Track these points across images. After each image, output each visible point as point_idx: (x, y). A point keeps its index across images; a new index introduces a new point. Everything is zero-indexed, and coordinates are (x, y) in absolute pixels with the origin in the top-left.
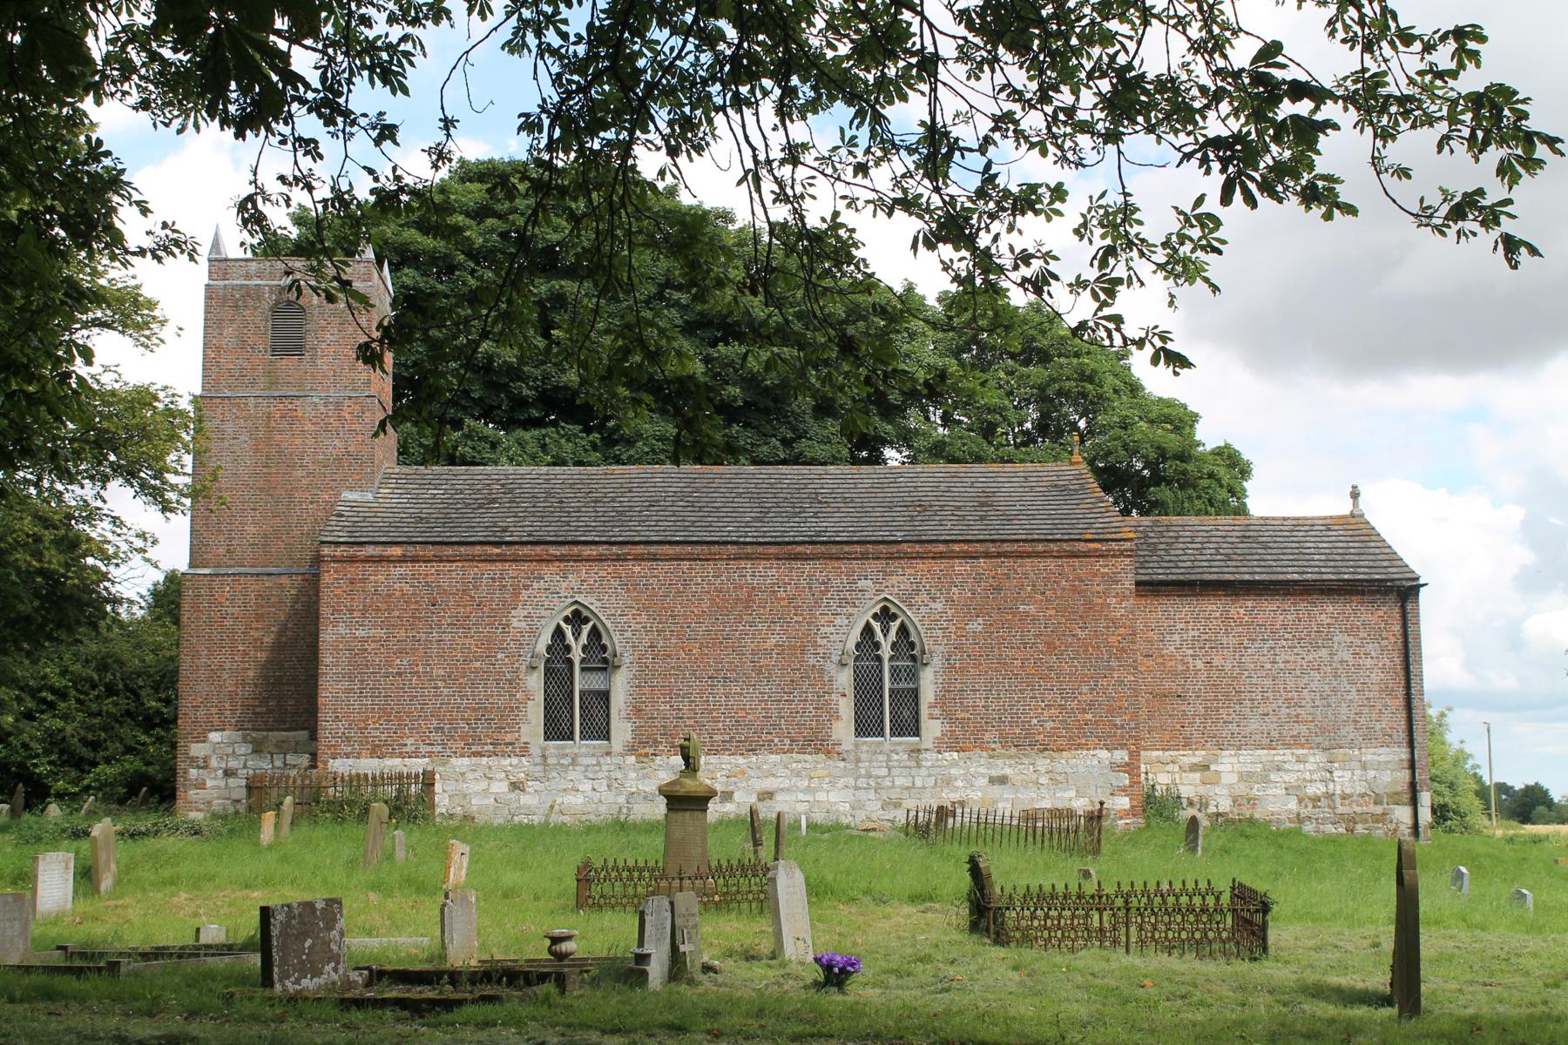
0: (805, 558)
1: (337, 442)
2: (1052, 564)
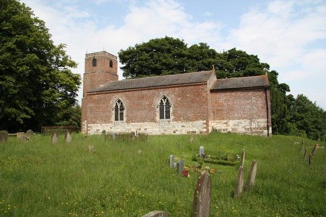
0: (152, 89)
2: (192, 87)
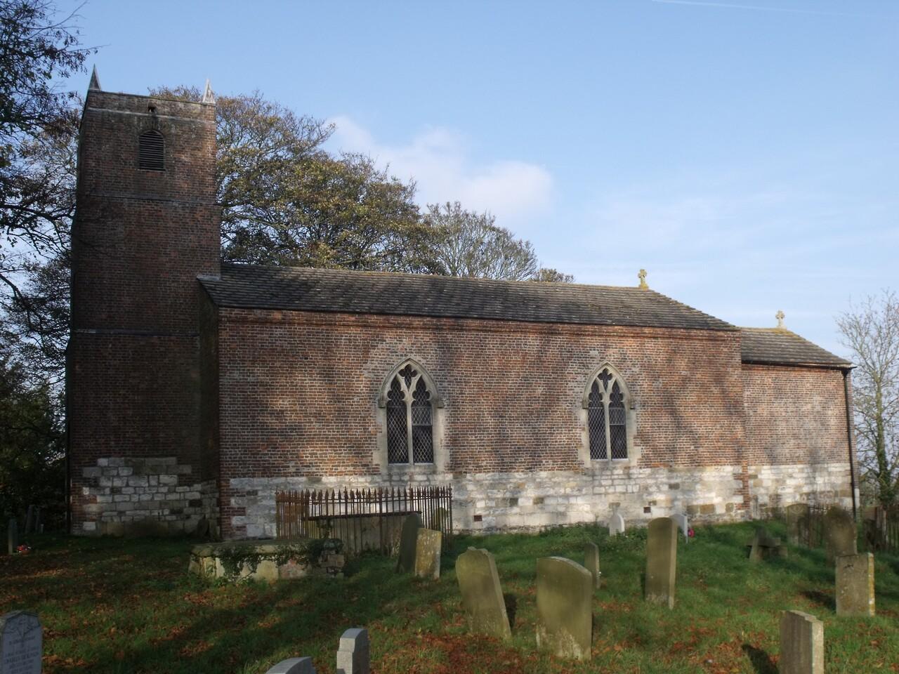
1: (192, 237)
